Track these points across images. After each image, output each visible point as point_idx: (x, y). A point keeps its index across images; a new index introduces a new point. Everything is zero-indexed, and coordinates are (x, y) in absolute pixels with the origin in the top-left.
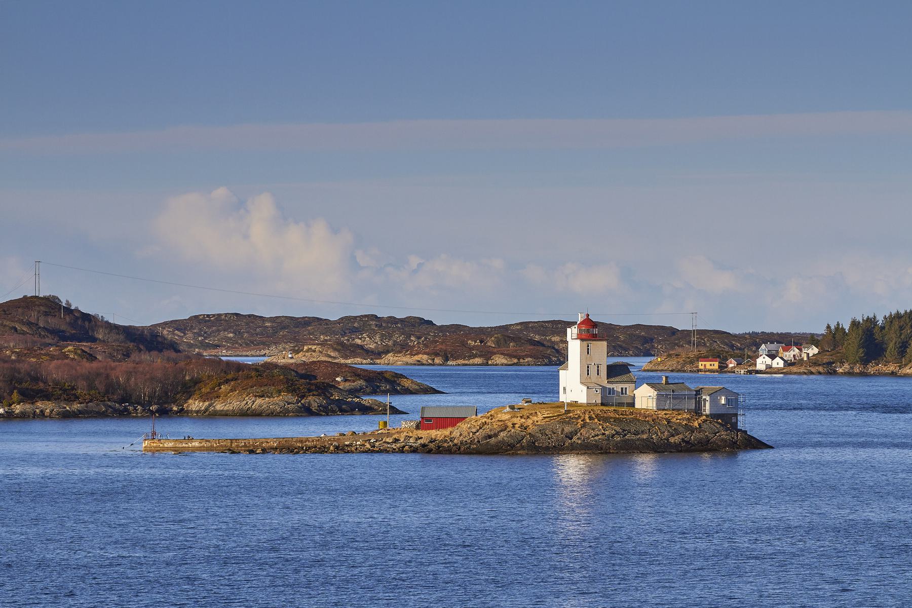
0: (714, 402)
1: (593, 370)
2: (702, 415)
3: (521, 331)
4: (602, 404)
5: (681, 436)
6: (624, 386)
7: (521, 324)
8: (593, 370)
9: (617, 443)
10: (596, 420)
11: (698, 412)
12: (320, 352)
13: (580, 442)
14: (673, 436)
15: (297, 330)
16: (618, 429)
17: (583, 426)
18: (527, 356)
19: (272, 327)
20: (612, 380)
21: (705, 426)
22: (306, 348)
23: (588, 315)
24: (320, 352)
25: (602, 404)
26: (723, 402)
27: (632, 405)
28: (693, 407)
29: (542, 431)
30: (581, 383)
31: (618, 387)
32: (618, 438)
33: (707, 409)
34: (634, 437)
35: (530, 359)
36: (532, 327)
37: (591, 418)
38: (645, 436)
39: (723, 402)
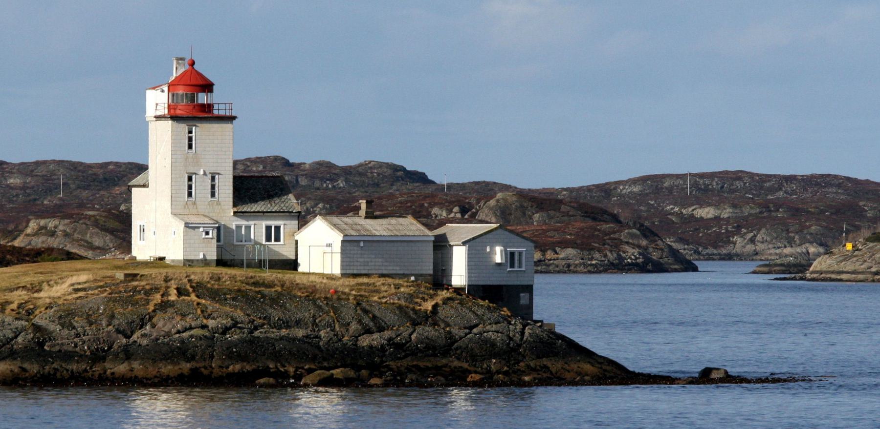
0: (476, 260)
1: (201, 186)
2: (449, 286)
3: (641, 197)
4: (220, 262)
5: (387, 334)
6: (273, 223)
7: (643, 180)
8: (201, 186)
9: (231, 345)
10: (193, 297)
11: (439, 277)
12: (66, 235)
13: (145, 342)
14: (369, 331)
15: (85, 194)
16: (239, 314)
17: (164, 306)
18: (565, 244)
19: (24, 188)
20: (246, 208)
21: (442, 313)
22: (33, 225)
23: (193, 63)
24: (66, 235)
25: (220, 262)
26: (498, 259)
27: (293, 265)
28: (429, 269)
29: (66, 317)
30: (174, 214)
31: (257, 230)
32: (234, 336)
33: (459, 276)
34: (274, 333)
35: (570, 251)
36: (670, 190)
37: (180, 292)
38: (300, 333)
39: (498, 259)
